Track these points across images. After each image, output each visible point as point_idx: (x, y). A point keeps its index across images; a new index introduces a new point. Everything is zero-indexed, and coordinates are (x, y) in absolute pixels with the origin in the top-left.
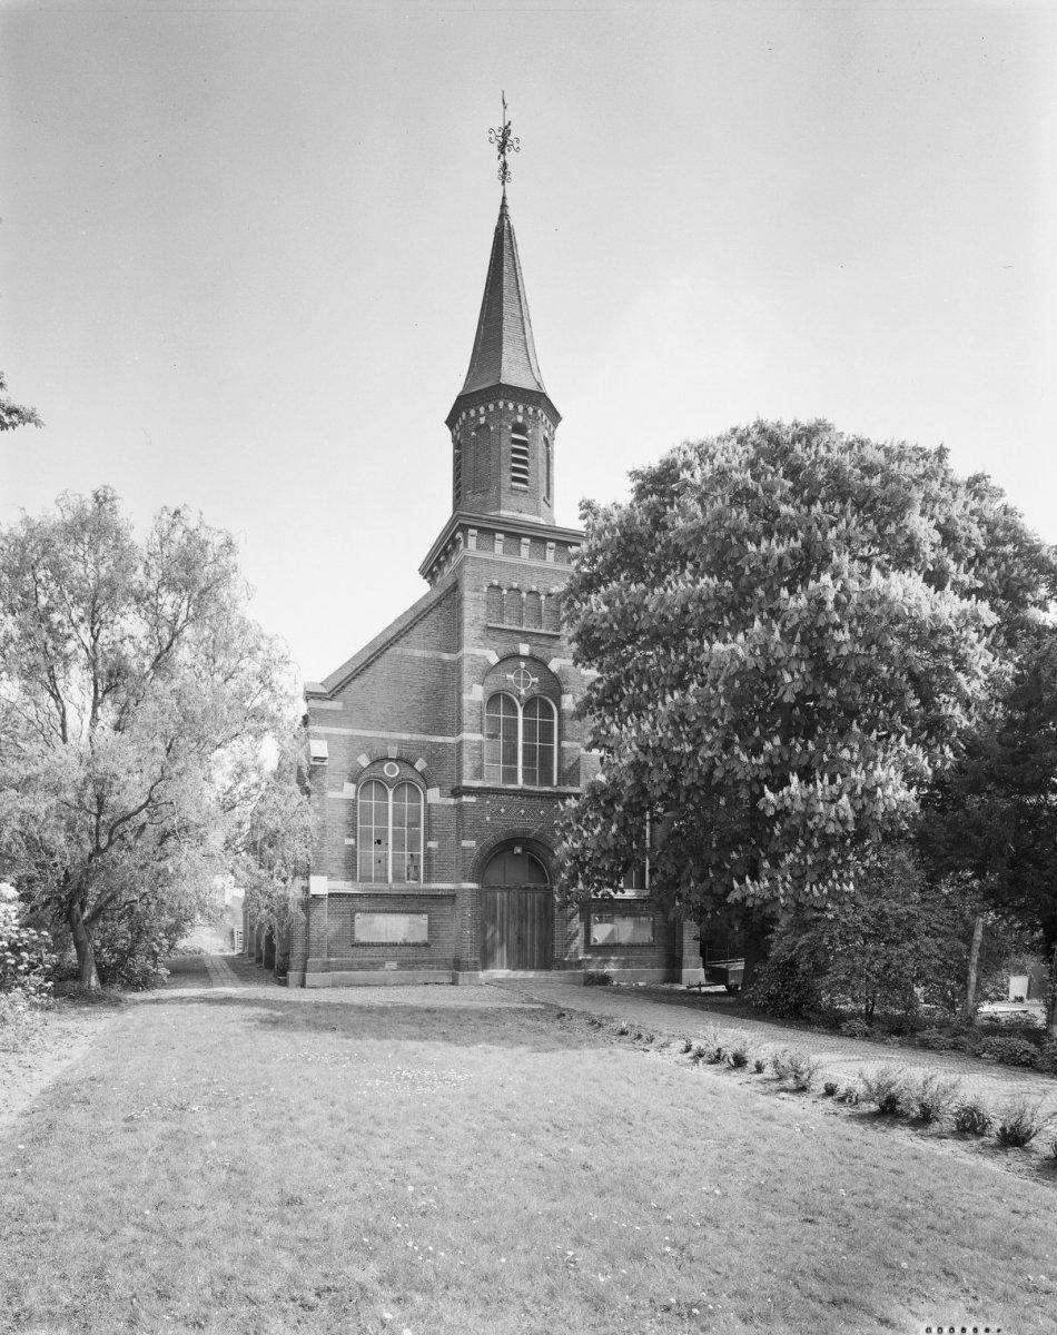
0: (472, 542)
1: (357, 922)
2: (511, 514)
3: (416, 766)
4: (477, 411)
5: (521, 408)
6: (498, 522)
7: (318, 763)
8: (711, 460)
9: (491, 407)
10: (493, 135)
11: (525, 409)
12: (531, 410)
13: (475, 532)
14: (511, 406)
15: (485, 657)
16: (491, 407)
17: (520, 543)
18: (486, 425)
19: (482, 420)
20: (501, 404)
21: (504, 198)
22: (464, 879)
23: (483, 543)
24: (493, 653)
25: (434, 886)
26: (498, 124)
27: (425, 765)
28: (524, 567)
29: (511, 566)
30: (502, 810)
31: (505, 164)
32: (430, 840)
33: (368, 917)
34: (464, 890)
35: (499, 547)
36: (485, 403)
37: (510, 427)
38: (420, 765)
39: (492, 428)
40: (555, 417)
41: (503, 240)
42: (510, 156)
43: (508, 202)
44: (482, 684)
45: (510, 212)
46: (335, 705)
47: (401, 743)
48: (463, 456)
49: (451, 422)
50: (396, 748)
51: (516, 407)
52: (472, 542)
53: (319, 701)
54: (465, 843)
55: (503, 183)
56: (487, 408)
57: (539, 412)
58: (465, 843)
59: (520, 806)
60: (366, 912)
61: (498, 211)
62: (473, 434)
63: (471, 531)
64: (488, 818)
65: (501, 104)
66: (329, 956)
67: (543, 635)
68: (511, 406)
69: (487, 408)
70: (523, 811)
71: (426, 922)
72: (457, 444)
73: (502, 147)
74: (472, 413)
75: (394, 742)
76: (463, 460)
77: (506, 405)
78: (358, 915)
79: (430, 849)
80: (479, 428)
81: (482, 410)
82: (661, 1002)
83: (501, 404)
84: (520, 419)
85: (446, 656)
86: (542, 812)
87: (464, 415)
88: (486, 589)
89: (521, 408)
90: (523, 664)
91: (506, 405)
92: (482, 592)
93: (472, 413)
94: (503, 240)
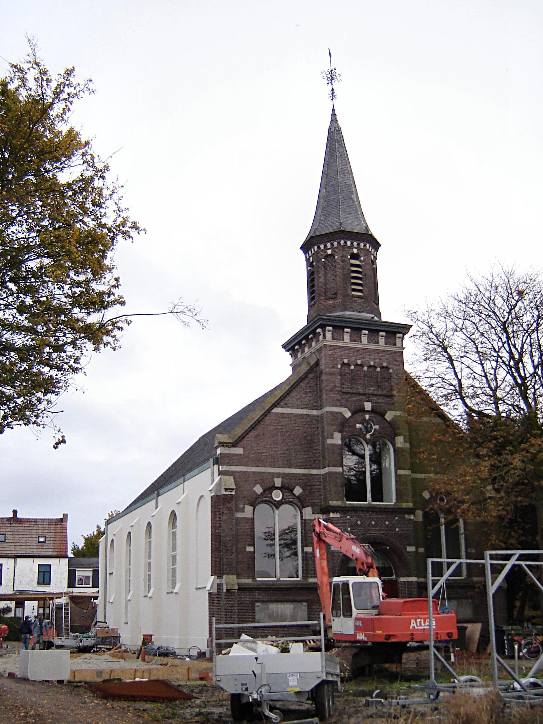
0: (329, 335)
1: (257, 609)
2: (353, 313)
3: (294, 492)
4: (325, 246)
5: (355, 244)
7: (228, 493)
8: (525, 469)
9: (335, 244)
10: (324, 74)
11: (358, 244)
12: (362, 245)
14: (349, 243)
15: (341, 413)
16: (335, 244)
20: (342, 242)
21: (333, 109)
23: (336, 336)
26: (327, 68)
27: (301, 490)
28: (365, 349)
29: (358, 350)
30: (359, 522)
31: (333, 90)
32: (306, 546)
35: (347, 338)
36: (331, 240)
37: (349, 257)
38: (298, 491)
39: (336, 257)
40: (376, 245)
41: (335, 138)
42: (336, 85)
43: (336, 113)
44: (340, 432)
46: (239, 451)
47: (284, 476)
48: (316, 273)
49: (305, 248)
50: (280, 479)
51: (352, 244)
52: (329, 335)
53: (227, 448)
55: (332, 99)
56: (332, 245)
57: (368, 245)
59: (371, 519)
60: (263, 602)
62: (323, 260)
63: (328, 328)
65: (332, 54)
67: (380, 395)
68: (349, 243)
69: (332, 245)
70: (373, 523)
72: (310, 264)
73: (331, 80)
74: (322, 247)
75: (278, 475)
76: (315, 276)
77: (345, 243)
78: (257, 604)
79: (306, 553)
80: (327, 256)
81: (329, 245)
82: (385, 508)
83: (342, 242)
84: (355, 251)
85: (314, 412)
86: (387, 523)
87: (316, 248)
88: (339, 366)
89: (355, 244)
90: (367, 417)
91: (345, 243)
92: (337, 368)
93: (322, 247)
94: (335, 138)
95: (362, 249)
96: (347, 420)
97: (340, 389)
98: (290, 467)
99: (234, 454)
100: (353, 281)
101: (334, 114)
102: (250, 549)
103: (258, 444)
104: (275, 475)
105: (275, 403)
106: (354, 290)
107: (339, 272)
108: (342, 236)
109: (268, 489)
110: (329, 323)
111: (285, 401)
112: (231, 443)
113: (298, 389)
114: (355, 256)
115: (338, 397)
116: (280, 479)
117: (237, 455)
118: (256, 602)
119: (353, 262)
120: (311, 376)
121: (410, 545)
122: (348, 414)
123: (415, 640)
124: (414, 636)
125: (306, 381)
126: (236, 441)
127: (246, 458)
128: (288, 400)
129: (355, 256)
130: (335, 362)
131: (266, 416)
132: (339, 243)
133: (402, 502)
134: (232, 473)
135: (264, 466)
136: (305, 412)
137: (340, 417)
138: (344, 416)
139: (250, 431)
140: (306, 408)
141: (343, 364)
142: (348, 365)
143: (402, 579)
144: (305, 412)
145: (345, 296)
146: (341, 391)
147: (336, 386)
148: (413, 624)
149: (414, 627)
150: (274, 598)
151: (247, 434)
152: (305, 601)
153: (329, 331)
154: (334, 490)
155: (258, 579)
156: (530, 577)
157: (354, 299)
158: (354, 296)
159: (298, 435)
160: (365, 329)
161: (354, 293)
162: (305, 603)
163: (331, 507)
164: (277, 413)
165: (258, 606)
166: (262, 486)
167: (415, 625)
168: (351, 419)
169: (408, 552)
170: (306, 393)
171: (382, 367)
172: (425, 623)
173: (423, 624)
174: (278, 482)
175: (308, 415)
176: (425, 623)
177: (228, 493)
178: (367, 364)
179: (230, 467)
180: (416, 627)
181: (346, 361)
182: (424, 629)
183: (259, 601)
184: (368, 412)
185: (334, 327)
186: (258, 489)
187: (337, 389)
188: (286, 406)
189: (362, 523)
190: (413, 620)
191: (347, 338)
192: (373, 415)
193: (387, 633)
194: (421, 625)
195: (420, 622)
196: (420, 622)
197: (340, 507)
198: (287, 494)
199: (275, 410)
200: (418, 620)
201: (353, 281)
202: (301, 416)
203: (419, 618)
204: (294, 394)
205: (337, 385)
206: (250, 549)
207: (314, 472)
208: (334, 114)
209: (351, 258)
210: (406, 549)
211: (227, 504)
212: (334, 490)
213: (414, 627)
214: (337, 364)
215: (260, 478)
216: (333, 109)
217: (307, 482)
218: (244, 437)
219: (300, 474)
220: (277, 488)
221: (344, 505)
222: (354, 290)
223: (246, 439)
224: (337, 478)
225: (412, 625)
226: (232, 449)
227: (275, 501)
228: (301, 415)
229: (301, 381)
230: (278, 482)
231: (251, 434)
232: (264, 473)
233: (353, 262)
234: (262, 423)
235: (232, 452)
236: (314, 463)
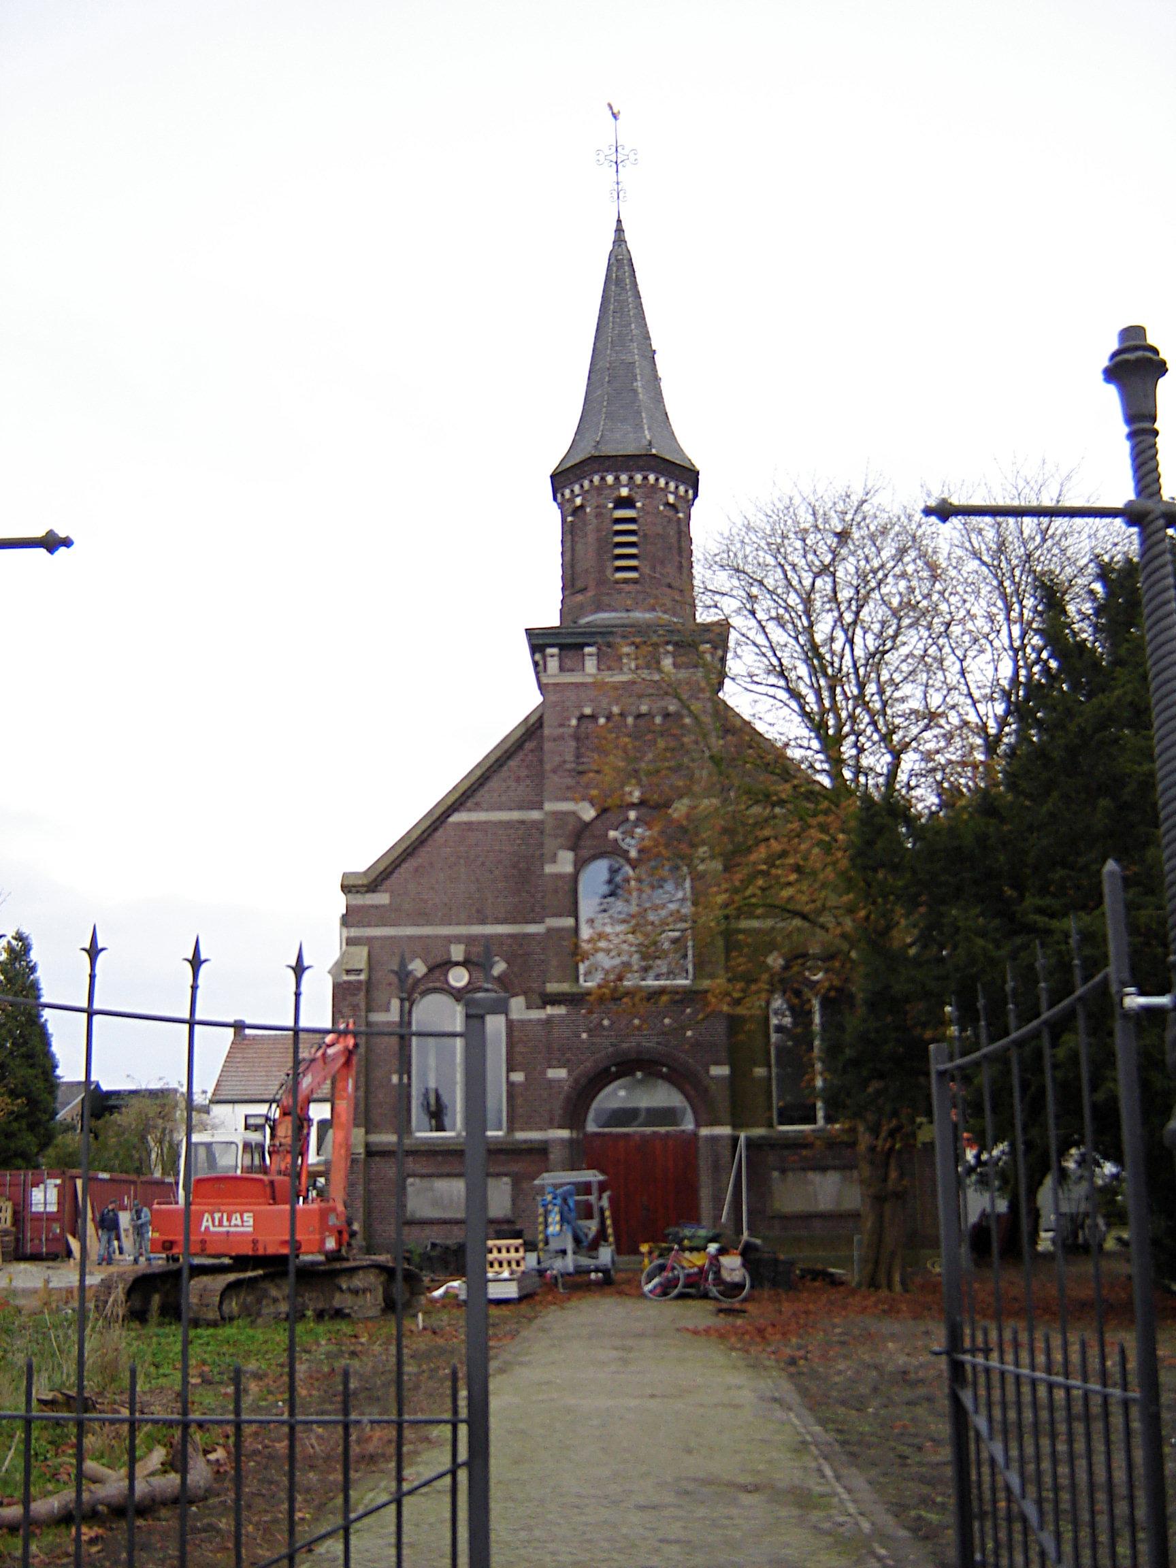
1: (410, 1189)
2: (613, 615)
6: (574, 634)
7: (352, 978)
9: (586, 484)
13: (555, 651)
14: (610, 479)
17: (584, 655)
18: (582, 507)
19: (578, 501)
21: (619, 221)
22: (551, 1124)
23: (568, 663)
24: (586, 805)
25: (520, 1135)
30: (606, 1022)
33: (425, 1183)
34: (554, 1140)
38: (499, 968)
40: (689, 476)
43: (625, 226)
45: (628, 236)
46: (381, 898)
47: (470, 940)
50: (462, 947)
51: (617, 479)
53: (359, 896)
54: (552, 1073)
58: (552, 1073)
60: (422, 1176)
61: (611, 236)
63: (550, 651)
64: (584, 1036)
66: (735, 1140)
68: (610, 479)
71: (508, 1188)
72: (570, 533)
75: (457, 939)
77: (603, 479)
78: (410, 1180)
81: (577, 488)
84: (624, 492)
86: (667, 1021)
88: (574, 722)
89: (624, 478)
90: (632, 815)
95: (639, 486)
96: (587, 825)
97: (573, 765)
98: (483, 922)
99: (372, 906)
100: (618, 551)
101: (619, 230)
102: (518, 1077)
103: (419, 884)
104: (450, 940)
105: (454, 803)
106: (619, 569)
107: (591, 538)
108: (596, 466)
109: (438, 966)
110: (548, 641)
111: (478, 797)
112: (363, 886)
113: (504, 772)
114: (627, 503)
115: (570, 781)
116: (462, 947)
117: (377, 907)
118: (409, 1176)
119: (620, 514)
120: (529, 745)
121: (717, 1063)
122: (589, 813)
123: (208, 1252)
124: (208, 1245)
125: (521, 755)
126: (375, 879)
127: (396, 910)
128: (483, 795)
129: (627, 503)
130: (565, 714)
131: (435, 830)
132: (645, 478)
133: (703, 977)
134: (369, 941)
135: (429, 923)
136: (516, 815)
137: (571, 819)
138: (579, 819)
139: (404, 861)
140: (520, 808)
141: (582, 717)
142: (593, 717)
143: (704, 1131)
144: (516, 815)
145: (602, 582)
146: (573, 770)
147: (565, 762)
148: (206, 1222)
149: (207, 1228)
150: (446, 1169)
151: (399, 865)
152: (506, 1175)
153: (552, 656)
154: (554, 962)
155: (489, 1133)
156: (635, 1133)
157: (618, 586)
158: (617, 582)
159: (500, 862)
160: (552, 646)
161: (619, 575)
162: (506, 1179)
163: (551, 994)
164: (459, 824)
165: (412, 1184)
166: (425, 961)
167: (210, 1223)
168: (598, 822)
169: (712, 1078)
170: (518, 780)
171: (609, 718)
172: (229, 1220)
173: (225, 1223)
174: (457, 952)
175: (523, 822)
176: (229, 1220)
177: (352, 978)
178: (633, 708)
179: (362, 929)
180: (212, 1229)
181: (588, 711)
182: (228, 1232)
183: (414, 1175)
184: (632, 806)
185: (562, 647)
186: (418, 967)
187: (568, 766)
188: (478, 807)
189: (613, 1023)
190: (206, 1215)
191: (591, 665)
192: (644, 810)
193: (166, 1238)
194: (221, 1224)
195: (221, 1220)
196: (221, 1220)
197: (563, 994)
198: (479, 975)
199: (455, 818)
200: (217, 1216)
201: (618, 551)
202: (508, 824)
203: (219, 1211)
204: (494, 783)
205: (567, 758)
206: (518, 1077)
207: (532, 929)
208: (619, 230)
209: (616, 507)
210: (707, 1071)
211: (350, 998)
212: (554, 962)
213: (207, 1228)
214: (569, 719)
215: (422, 946)
216: (619, 221)
217: (517, 950)
218: (391, 873)
219: (501, 935)
220: (457, 964)
221: (575, 990)
222: (619, 569)
223: (395, 875)
224: (562, 938)
225: (205, 1224)
226: (368, 896)
227: (453, 988)
228: (508, 822)
229: (509, 758)
230: (457, 952)
231: (404, 866)
232: (428, 937)
233: (620, 514)
234: (430, 842)
235: (369, 902)
236: (533, 911)
